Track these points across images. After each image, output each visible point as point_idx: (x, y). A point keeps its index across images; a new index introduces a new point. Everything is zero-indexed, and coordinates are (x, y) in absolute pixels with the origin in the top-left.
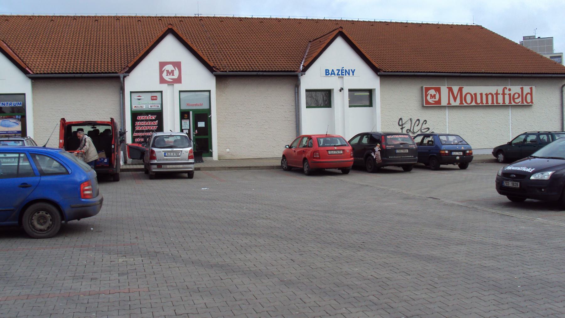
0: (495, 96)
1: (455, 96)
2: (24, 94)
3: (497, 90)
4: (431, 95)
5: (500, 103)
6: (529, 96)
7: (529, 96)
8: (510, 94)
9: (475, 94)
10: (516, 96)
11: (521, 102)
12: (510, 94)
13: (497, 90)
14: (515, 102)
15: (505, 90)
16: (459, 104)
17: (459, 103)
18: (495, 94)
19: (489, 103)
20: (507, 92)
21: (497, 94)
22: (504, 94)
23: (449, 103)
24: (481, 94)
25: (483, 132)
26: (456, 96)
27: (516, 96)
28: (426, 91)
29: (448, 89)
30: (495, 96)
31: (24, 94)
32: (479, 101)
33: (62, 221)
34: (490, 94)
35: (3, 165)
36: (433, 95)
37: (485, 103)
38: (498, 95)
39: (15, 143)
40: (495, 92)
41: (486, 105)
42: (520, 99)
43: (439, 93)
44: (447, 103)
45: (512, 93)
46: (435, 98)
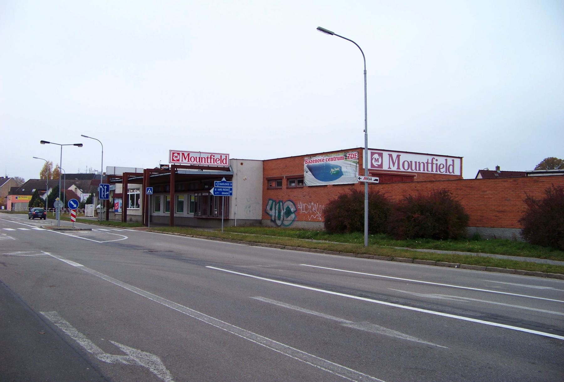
0: (426, 164)
1: (186, 157)
2: (107, 167)
3: (428, 159)
4: (175, 156)
5: (429, 171)
6: (451, 167)
7: (451, 167)
8: (437, 164)
9: (411, 162)
10: (442, 166)
11: (445, 172)
12: (437, 164)
13: (428, 159)
14: (440, 171)
15: (434, 159)
16: (387, 168)
17: (397, 168)
18: (426, 163)
19: (434, 171)
20: (435, 162)
21: (208, 158)
22: (211, 158)
23: (389, 168)
24: (416, 162)
25: (428, 190)
26: (394, 162)
27: (442, 166)
28: (173, 154)
29: (388, 156)
30: (426, 164)
31: (107, 167)
32: (414, 168)
33: (455, 268)
34: (423, 163)
35: (193, 213)
36: (377, 159)
37: (435, 171)
38: (434, 165)
39: (121, 204)
40: (426, 162)
41: (397, 170)
42: (444, 169)
43: (381, 158)
44: (388, 167)
45: (439, 163)
46: (378, 162)
